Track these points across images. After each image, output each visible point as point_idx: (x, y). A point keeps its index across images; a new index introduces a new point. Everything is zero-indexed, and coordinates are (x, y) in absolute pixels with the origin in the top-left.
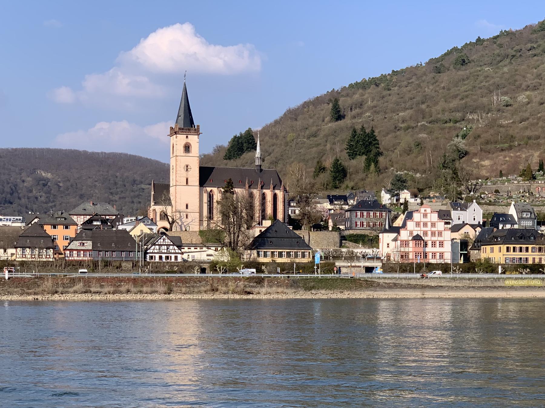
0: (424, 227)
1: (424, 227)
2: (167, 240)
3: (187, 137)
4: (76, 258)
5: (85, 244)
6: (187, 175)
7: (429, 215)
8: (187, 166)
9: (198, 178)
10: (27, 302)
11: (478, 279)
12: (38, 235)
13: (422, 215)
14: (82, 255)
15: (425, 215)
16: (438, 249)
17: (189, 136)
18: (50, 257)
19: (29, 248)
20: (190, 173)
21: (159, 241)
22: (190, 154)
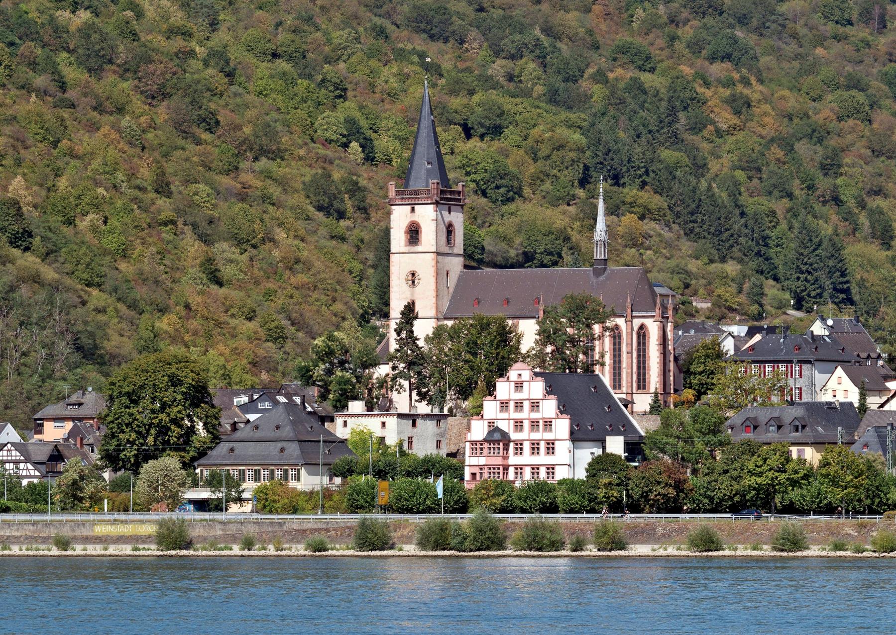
0: (515, 411)
1: (515, 411)
2: (14, 453)
3: (413, 210)
6: (412, 294)
7: (525, 385)
8: (413, 275)
11: (47, 524)
13: (513, 384)
15: (519, 386)
16: (542, 459)
17: (416, 207)
20: (418, 289)
22: (419, 248)
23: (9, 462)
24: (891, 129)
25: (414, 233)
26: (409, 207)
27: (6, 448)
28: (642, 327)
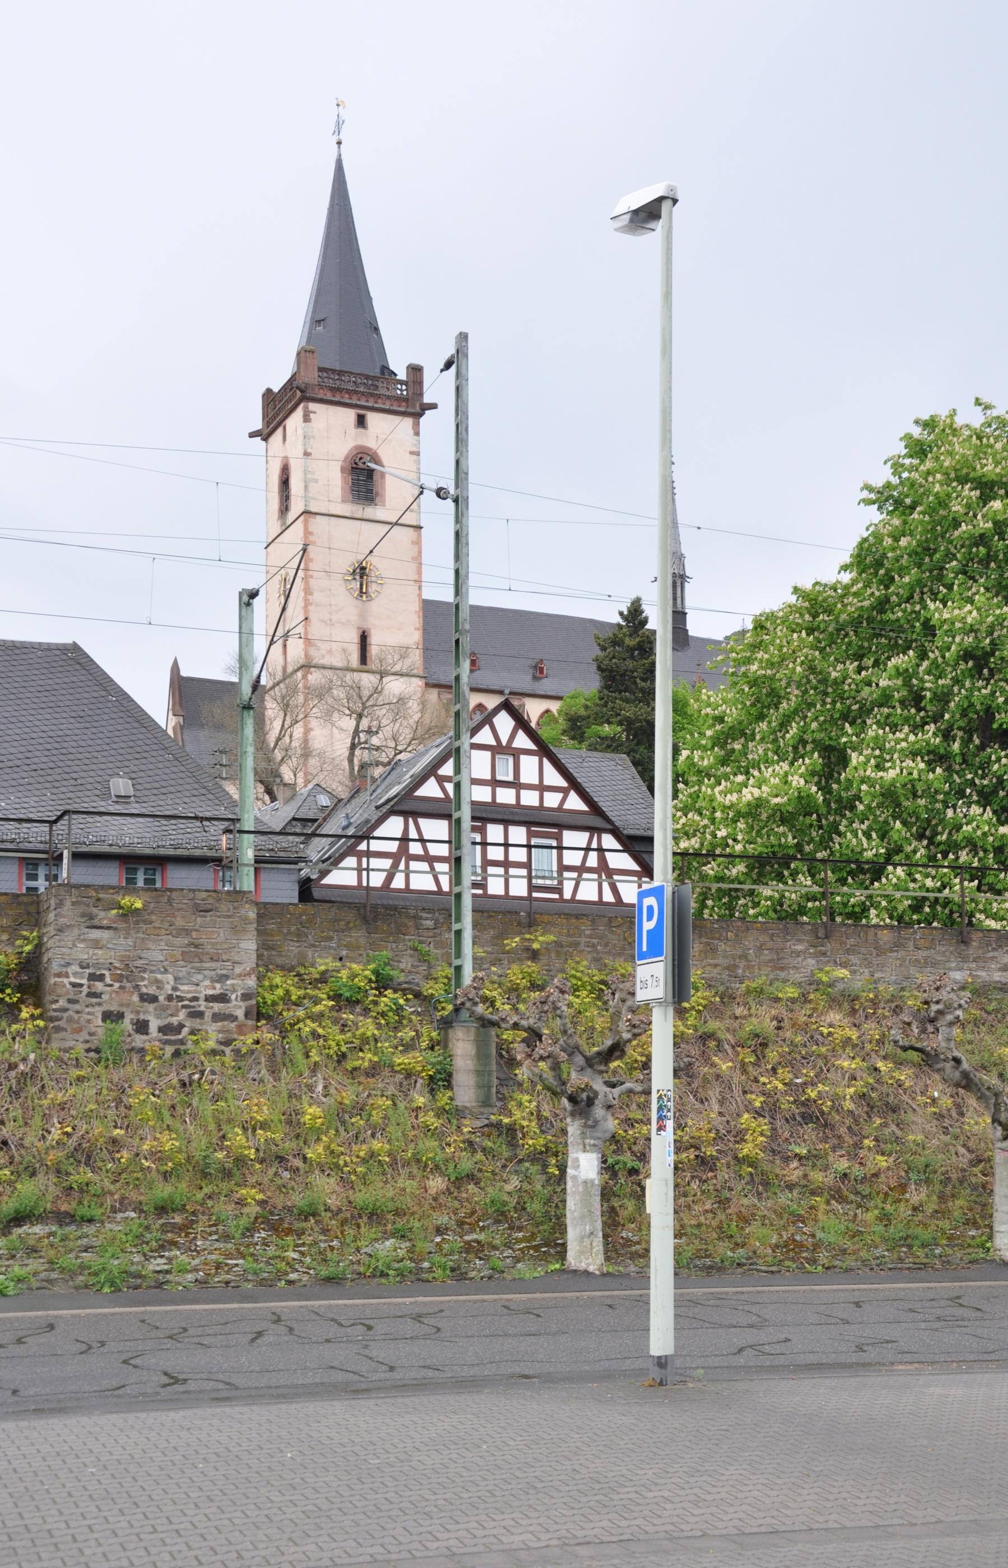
3: (361, 421)
6: (363, 615)
17: (372, 417)
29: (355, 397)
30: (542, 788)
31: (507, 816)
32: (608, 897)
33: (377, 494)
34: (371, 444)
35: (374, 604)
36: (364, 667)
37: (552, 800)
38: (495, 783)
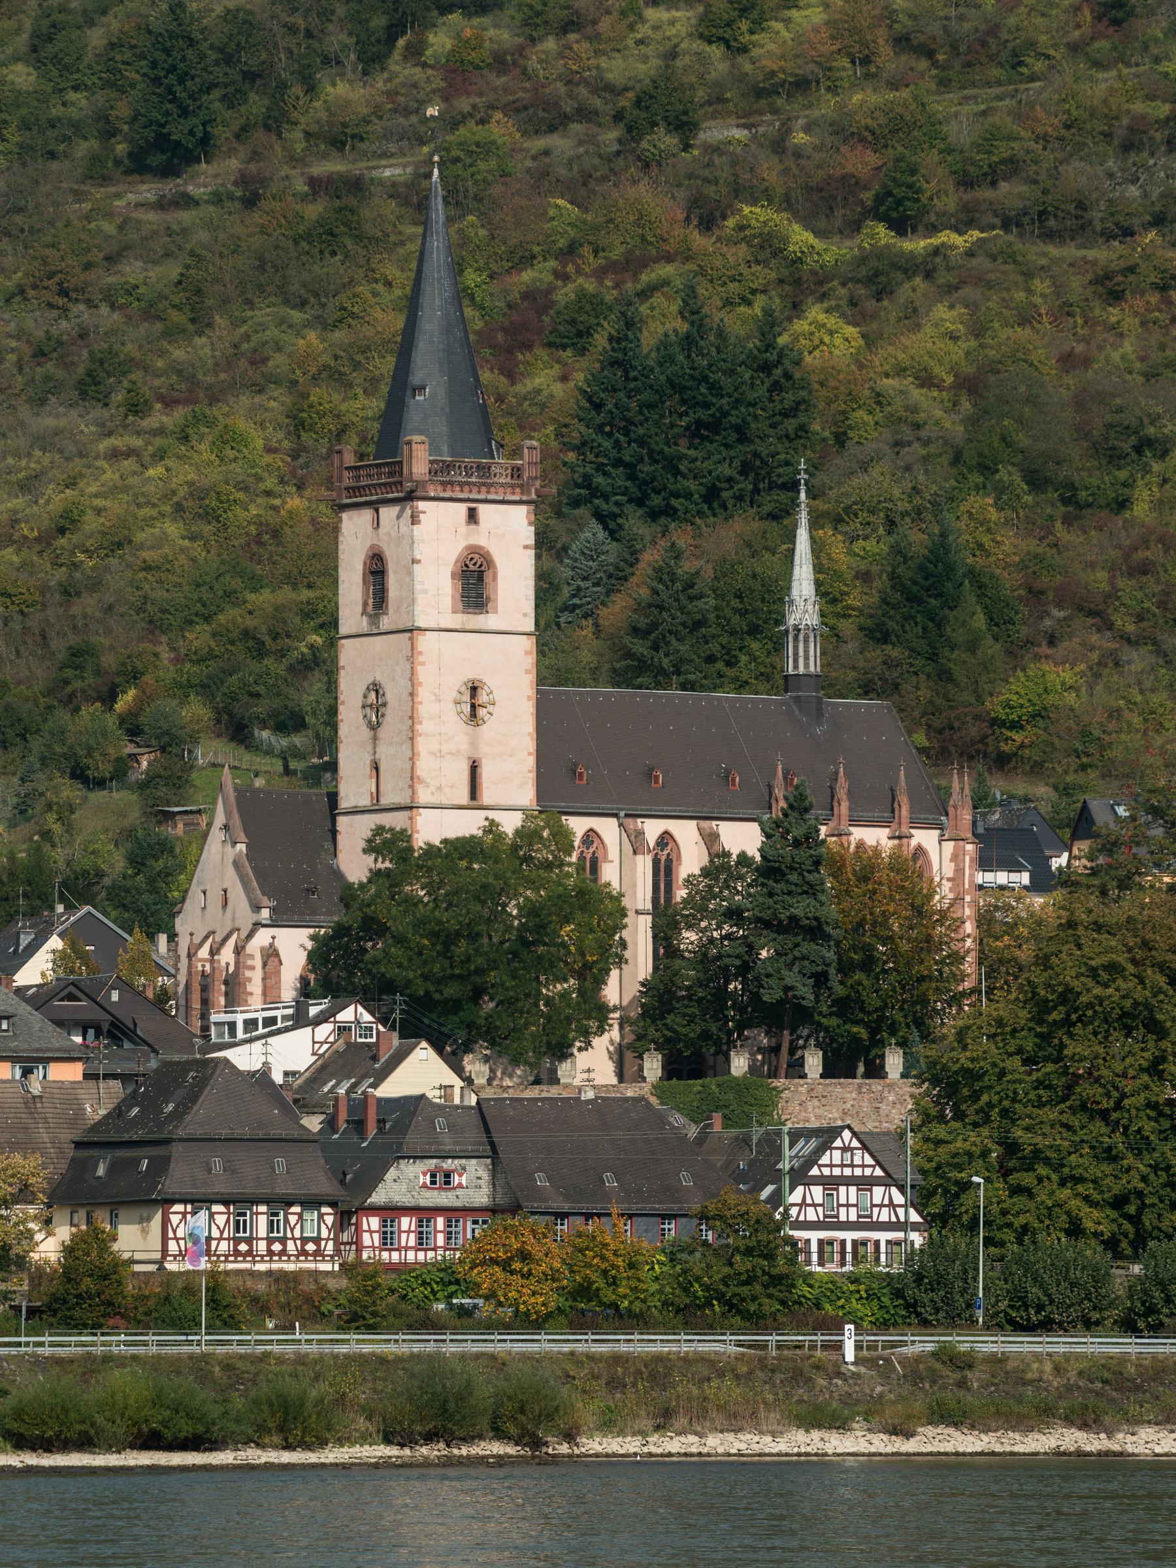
3: (472, 516)
4: (411, 1256)
5: (456, 1180)
6: (473, 744)
8: (474, 690)
9: (531, 762)
10: (427, 1464)
12: (247, 1132)
14: (441, 1240)
17: (484, 510)
18: (318, 1253)
19: (226, 1203)
20: (489, 729)
21: (825, 1160)
23: (848, 1181)
24: (520, 5)
25: (474, 581)
26: (463, 508)
27: (838, 1143)
28: (665, 839)
29: (466, 488)
30: (863, 1166)
31: (848, 1181)
32: (894, 1219)
33: (488, 599)
34: (482, 541)
35: (484, 728)
36: (475, 803)
37: (868, 1172)
38: (842, 1166)
